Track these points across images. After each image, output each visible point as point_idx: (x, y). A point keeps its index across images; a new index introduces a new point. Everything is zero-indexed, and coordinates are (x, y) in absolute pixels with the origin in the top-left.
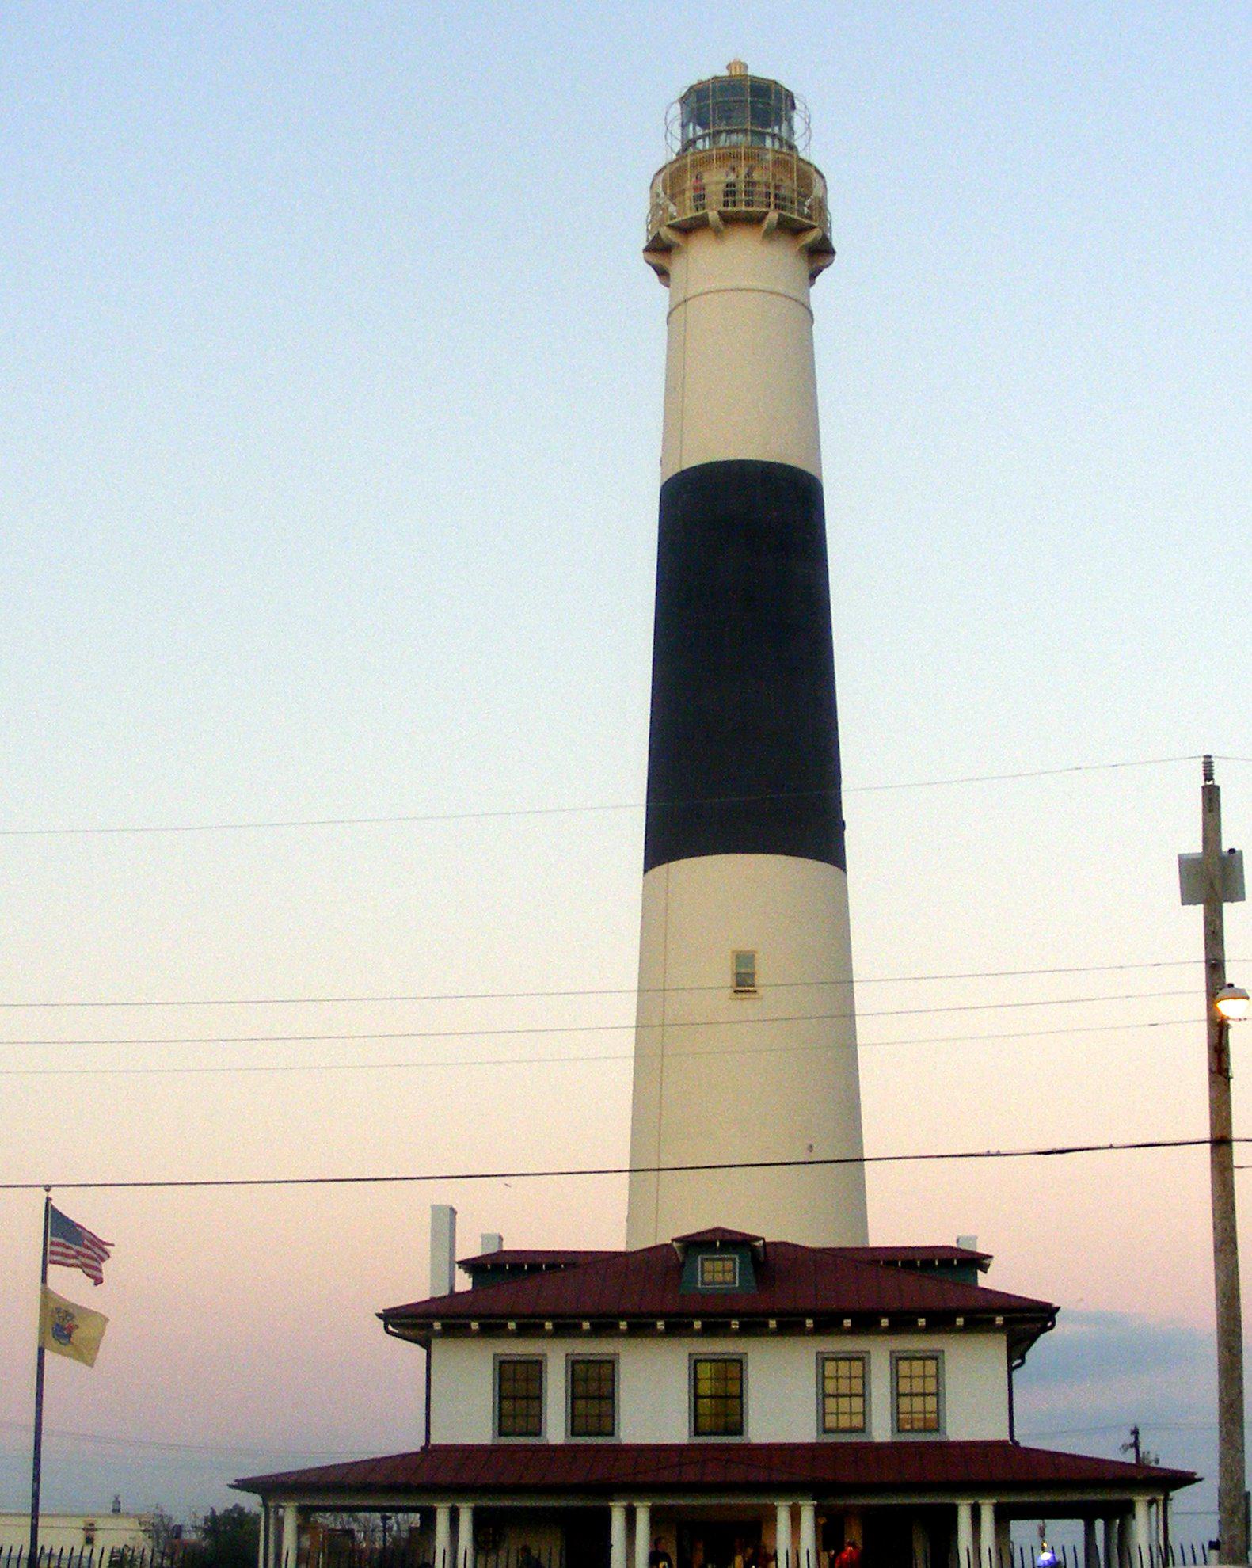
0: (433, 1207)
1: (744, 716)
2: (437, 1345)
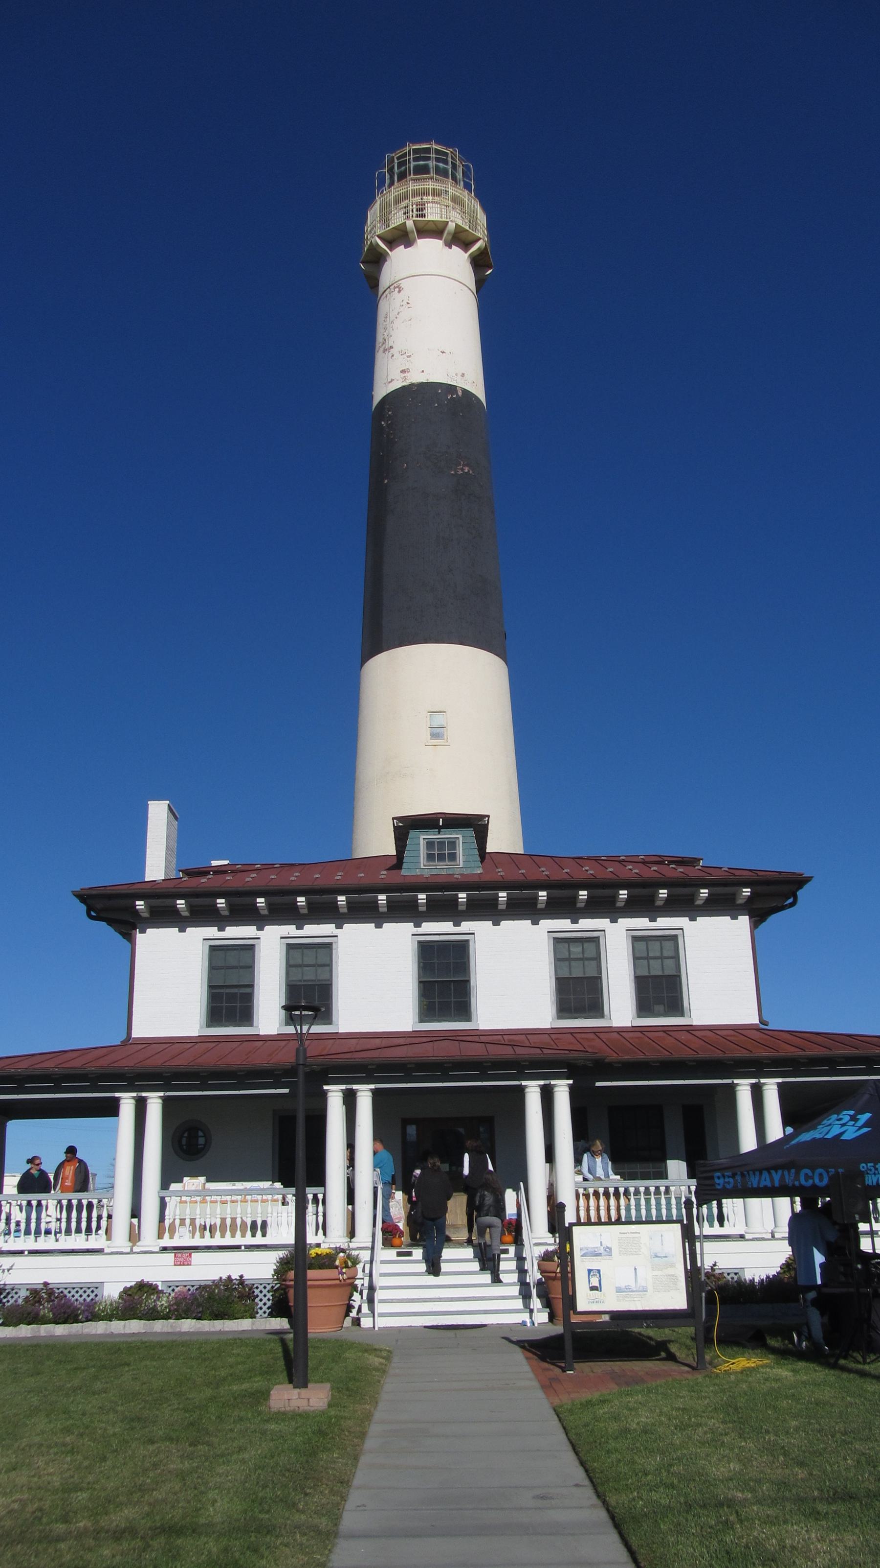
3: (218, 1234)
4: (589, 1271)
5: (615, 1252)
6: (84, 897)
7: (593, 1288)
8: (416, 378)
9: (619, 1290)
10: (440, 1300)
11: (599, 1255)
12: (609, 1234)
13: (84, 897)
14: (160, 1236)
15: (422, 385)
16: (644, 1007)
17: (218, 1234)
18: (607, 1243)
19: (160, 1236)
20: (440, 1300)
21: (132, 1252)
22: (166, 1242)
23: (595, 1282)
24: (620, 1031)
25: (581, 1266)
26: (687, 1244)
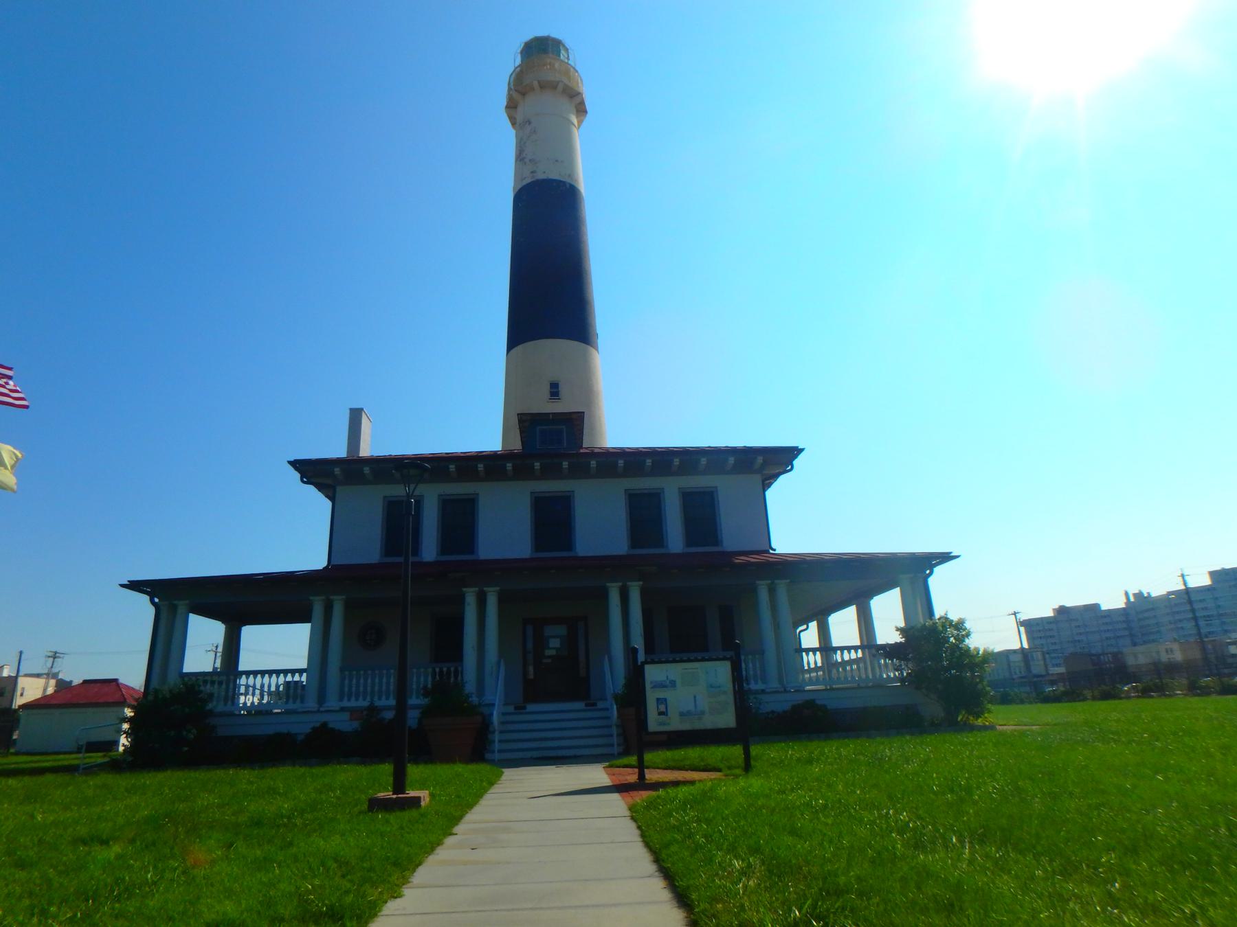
0: (351, 410)
1: (549, 293)
2: (341, 491)
3: (353, 699)
4: (658, 700)
5: (678, 683)
6: (297, 464)
7: (661, 713)
8: (541, 176)
9: (682, 714)
10: (563, 720)
11: (665, 686)
12: (673, 671)
13: (297, 464)
14: (341, 699)
15: (544, 180)
16: (690, 539)
17: (353, 699)
18: (672, 677)
19: (341, 699)
20: (563, 720)
21: (318, 711)
22: (345, 704)
23: (662, 708)
24: (678, 555)
25: (651, 697)
26: (503, 668)
